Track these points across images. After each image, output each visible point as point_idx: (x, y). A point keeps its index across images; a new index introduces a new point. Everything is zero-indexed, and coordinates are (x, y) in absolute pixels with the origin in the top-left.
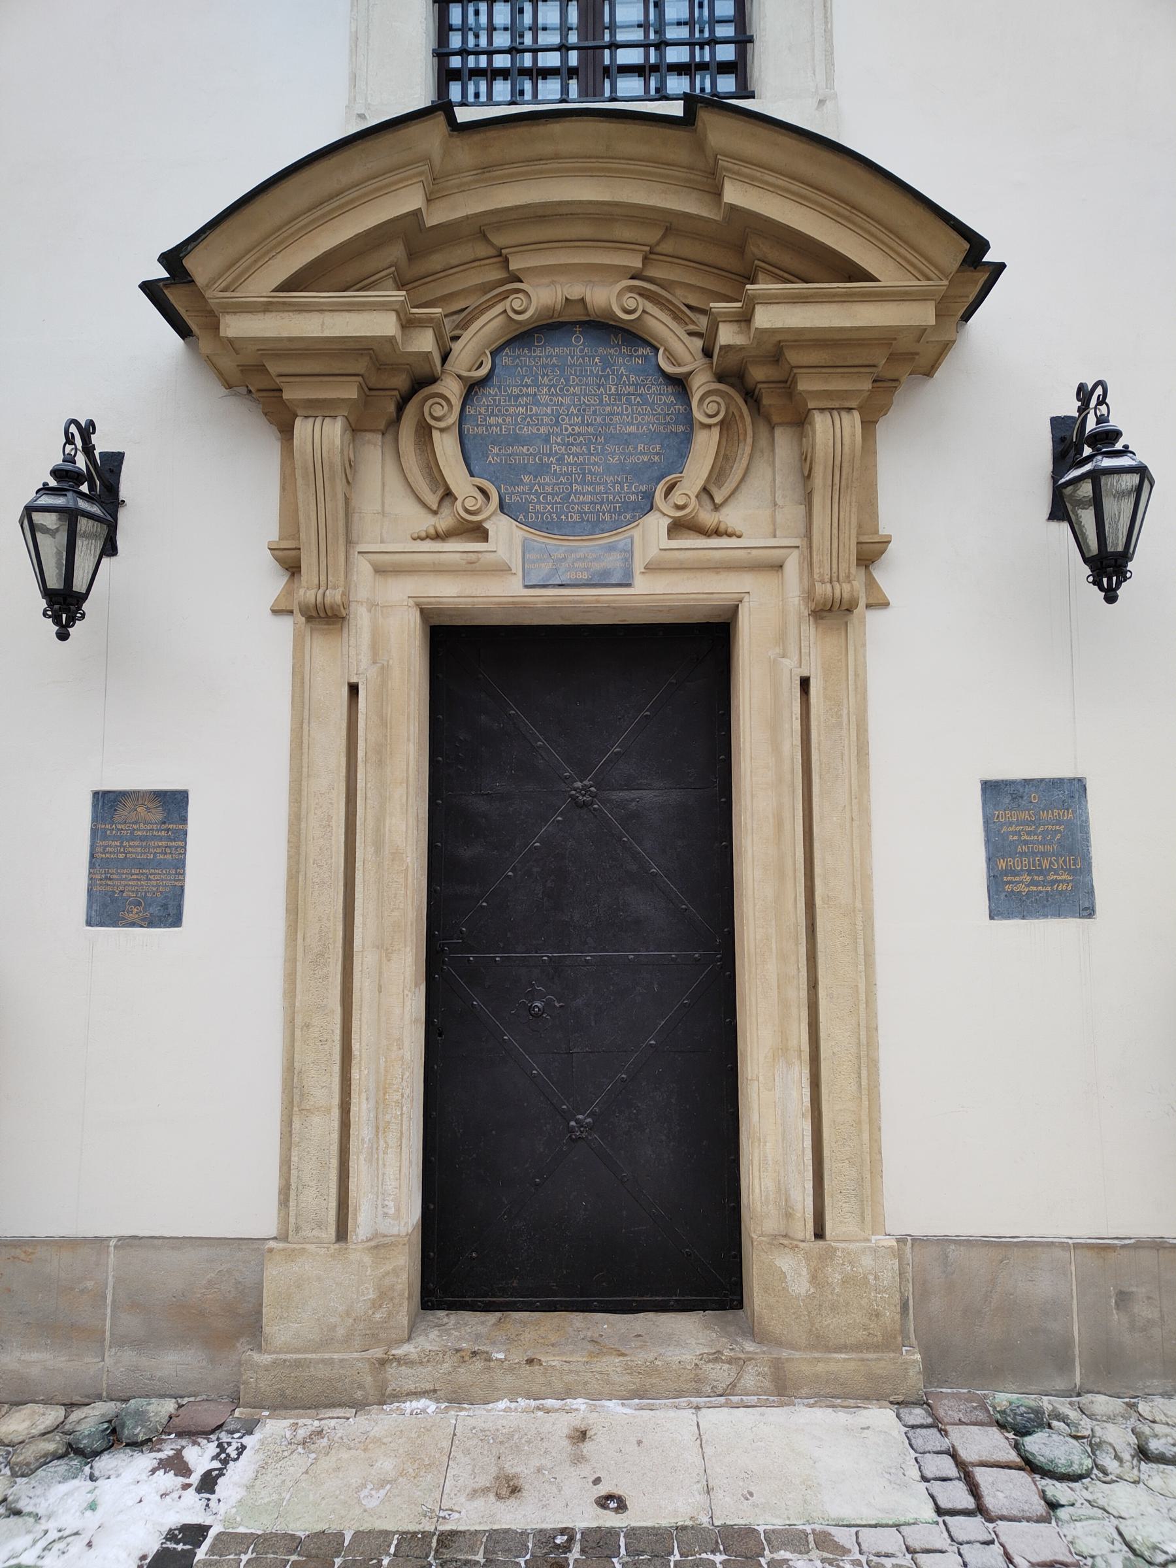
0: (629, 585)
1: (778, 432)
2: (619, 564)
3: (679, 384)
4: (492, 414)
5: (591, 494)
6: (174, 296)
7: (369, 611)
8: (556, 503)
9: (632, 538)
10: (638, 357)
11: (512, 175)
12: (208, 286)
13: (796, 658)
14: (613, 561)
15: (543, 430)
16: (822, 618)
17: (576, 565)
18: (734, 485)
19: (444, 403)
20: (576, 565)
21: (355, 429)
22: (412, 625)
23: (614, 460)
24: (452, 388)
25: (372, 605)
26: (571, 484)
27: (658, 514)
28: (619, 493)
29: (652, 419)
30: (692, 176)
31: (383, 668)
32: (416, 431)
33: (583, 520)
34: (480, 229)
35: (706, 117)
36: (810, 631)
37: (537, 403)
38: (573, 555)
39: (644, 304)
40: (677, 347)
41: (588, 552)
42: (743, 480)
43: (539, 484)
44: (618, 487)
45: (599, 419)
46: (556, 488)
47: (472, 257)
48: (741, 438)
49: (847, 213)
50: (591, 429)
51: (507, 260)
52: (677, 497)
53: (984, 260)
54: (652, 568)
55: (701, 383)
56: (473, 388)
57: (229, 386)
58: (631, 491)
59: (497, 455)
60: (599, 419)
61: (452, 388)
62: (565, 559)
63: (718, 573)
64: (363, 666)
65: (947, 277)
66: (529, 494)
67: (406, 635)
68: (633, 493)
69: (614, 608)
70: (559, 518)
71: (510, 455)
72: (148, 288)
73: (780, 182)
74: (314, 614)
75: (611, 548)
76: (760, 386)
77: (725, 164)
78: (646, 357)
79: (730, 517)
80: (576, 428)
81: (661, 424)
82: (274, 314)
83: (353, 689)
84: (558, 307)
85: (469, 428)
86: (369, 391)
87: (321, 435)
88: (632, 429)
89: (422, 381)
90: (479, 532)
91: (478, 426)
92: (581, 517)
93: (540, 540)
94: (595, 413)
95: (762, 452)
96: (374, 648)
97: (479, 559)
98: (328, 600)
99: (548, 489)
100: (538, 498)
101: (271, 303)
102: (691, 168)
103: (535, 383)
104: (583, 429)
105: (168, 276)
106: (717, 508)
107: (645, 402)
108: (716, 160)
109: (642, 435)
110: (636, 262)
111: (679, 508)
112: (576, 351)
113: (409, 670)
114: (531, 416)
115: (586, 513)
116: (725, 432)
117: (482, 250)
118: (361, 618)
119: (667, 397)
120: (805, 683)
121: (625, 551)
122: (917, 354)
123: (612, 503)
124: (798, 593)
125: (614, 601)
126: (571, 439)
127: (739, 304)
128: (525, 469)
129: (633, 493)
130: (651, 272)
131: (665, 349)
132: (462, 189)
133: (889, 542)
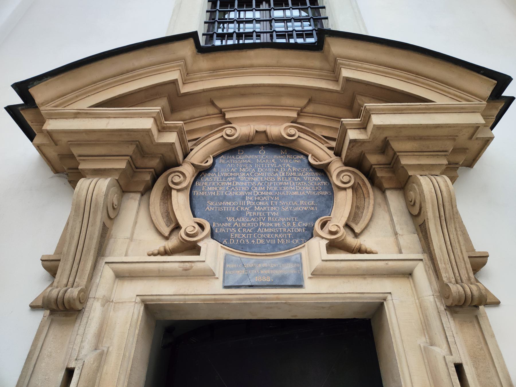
0: (300, 286)
1: (388, 193)
2: (293, 272)
3: (322, 171)
4: (211, 186)
5: (271, 227)
6: (27, 116)
7: (103, 305)
8: (249, 233)
9: (301, 255)
10: (297, 159)
11: (228, 74)
12: (43, 104)
13: (445, 346)
14: (288, 269)
15: (242, 193)
16: (456, 312)
17: (262, 272)
18: (366, 222)
19: (181, 175)
20: (262, 272)
21: (124, 188)
22: (135, 316)
23: (286, 209)
24: (187, 170)
25: (107, 301)
26: (258, 222)
27: (318, 238)
28: (290, 227)
29: (307, 188)
30: (322, 73)
31: (102, 354)
32: (163, 192)
33: (266, 243)
34: (209, 98)
35: (330, 41)
36: (450, 323)
37: (238, 180)
38: (260, 265)
39: (298, 134)
40: (320, 153)
41: (268, 265)
42: (371, 220)
43: (238, 222)
44: (289, 224)
45: (275, 188)
46: (249, 224)
47: (206, 113)
48: (366, 196)
49: (414, 78)
50: (271, 193)
51: (224, 115)
52: (331, 227)
53: (503, 94)
54: (317, 274)
55: (336, 166)
56: (201, 172)
57: (56, 171)
58: (300, 226)
59: (212, 206)
60: (275, 188)
61: (187, 170)
62: (254, 267)
63: (365, 278)
64: (84, 352)
65: (484, 100)
66: (231, 228)
67: (128, 326)
68: (299, 227)
69: (290, 304)
70: (250, 241)
71: (220, 206)
72: (11, 110)
73: (372, 67)
74: (54, 307)
75: (287, 261)
76: (374, 166)
77: (341, 61)
78: (301, 160)
79: (366, 241)
80: (262, 193)
81: (314, 191)
82: (80, 119)
83: (70, 372)
84: (252, 134)
85: (196, 193)
86: (134, 168)
87: (97, 188)
88: (295, 193)
89: (170, 164)
90: (193, 248)
91: (202, 191)
92: (265, 241)
93: (236, 255)
94: (273, 185)
95: (380, 205)
96: (100, 336)
97: (192, 267)
98: (67, 295)
99: (244, 225)
100: (237, 230)
101: (79, 113)
102: (321, 69)
103: (238, 171)
104: (266, 193)
105: (23, 102)
106: (356, 235)
107: (303, 180)
108: (336, 61)
109: (302, 197)
110: (294, 115)
111: (332, 233)
112: (262, 157)
113: (124, 355)
114: (234, 187)
115: (268, 239)
116: (355, 193)
117: (211, 110)
118: (94, 312)
119: (315, 178)
120: (459, 368)
121: (297, 263)
122: (467, 149)
123: (285, 233)
124: (430, 292)
125: (290, 299)
126: (259, 198)
127: (359, 119)
128: (229, 214)
129: (299, 227)
130: (301, 121)
131: (313, 155)
132: (202, 79)
133: (487, 256)
